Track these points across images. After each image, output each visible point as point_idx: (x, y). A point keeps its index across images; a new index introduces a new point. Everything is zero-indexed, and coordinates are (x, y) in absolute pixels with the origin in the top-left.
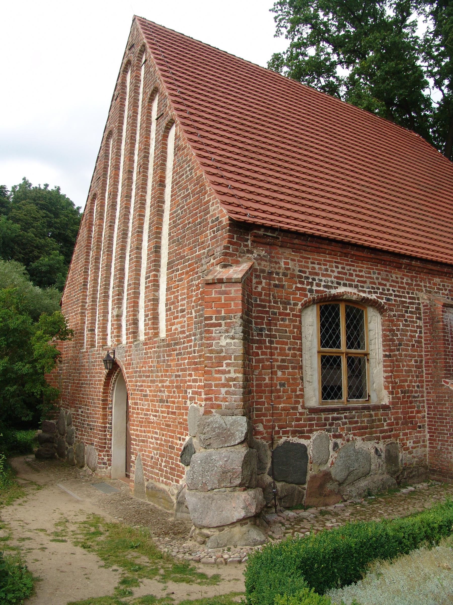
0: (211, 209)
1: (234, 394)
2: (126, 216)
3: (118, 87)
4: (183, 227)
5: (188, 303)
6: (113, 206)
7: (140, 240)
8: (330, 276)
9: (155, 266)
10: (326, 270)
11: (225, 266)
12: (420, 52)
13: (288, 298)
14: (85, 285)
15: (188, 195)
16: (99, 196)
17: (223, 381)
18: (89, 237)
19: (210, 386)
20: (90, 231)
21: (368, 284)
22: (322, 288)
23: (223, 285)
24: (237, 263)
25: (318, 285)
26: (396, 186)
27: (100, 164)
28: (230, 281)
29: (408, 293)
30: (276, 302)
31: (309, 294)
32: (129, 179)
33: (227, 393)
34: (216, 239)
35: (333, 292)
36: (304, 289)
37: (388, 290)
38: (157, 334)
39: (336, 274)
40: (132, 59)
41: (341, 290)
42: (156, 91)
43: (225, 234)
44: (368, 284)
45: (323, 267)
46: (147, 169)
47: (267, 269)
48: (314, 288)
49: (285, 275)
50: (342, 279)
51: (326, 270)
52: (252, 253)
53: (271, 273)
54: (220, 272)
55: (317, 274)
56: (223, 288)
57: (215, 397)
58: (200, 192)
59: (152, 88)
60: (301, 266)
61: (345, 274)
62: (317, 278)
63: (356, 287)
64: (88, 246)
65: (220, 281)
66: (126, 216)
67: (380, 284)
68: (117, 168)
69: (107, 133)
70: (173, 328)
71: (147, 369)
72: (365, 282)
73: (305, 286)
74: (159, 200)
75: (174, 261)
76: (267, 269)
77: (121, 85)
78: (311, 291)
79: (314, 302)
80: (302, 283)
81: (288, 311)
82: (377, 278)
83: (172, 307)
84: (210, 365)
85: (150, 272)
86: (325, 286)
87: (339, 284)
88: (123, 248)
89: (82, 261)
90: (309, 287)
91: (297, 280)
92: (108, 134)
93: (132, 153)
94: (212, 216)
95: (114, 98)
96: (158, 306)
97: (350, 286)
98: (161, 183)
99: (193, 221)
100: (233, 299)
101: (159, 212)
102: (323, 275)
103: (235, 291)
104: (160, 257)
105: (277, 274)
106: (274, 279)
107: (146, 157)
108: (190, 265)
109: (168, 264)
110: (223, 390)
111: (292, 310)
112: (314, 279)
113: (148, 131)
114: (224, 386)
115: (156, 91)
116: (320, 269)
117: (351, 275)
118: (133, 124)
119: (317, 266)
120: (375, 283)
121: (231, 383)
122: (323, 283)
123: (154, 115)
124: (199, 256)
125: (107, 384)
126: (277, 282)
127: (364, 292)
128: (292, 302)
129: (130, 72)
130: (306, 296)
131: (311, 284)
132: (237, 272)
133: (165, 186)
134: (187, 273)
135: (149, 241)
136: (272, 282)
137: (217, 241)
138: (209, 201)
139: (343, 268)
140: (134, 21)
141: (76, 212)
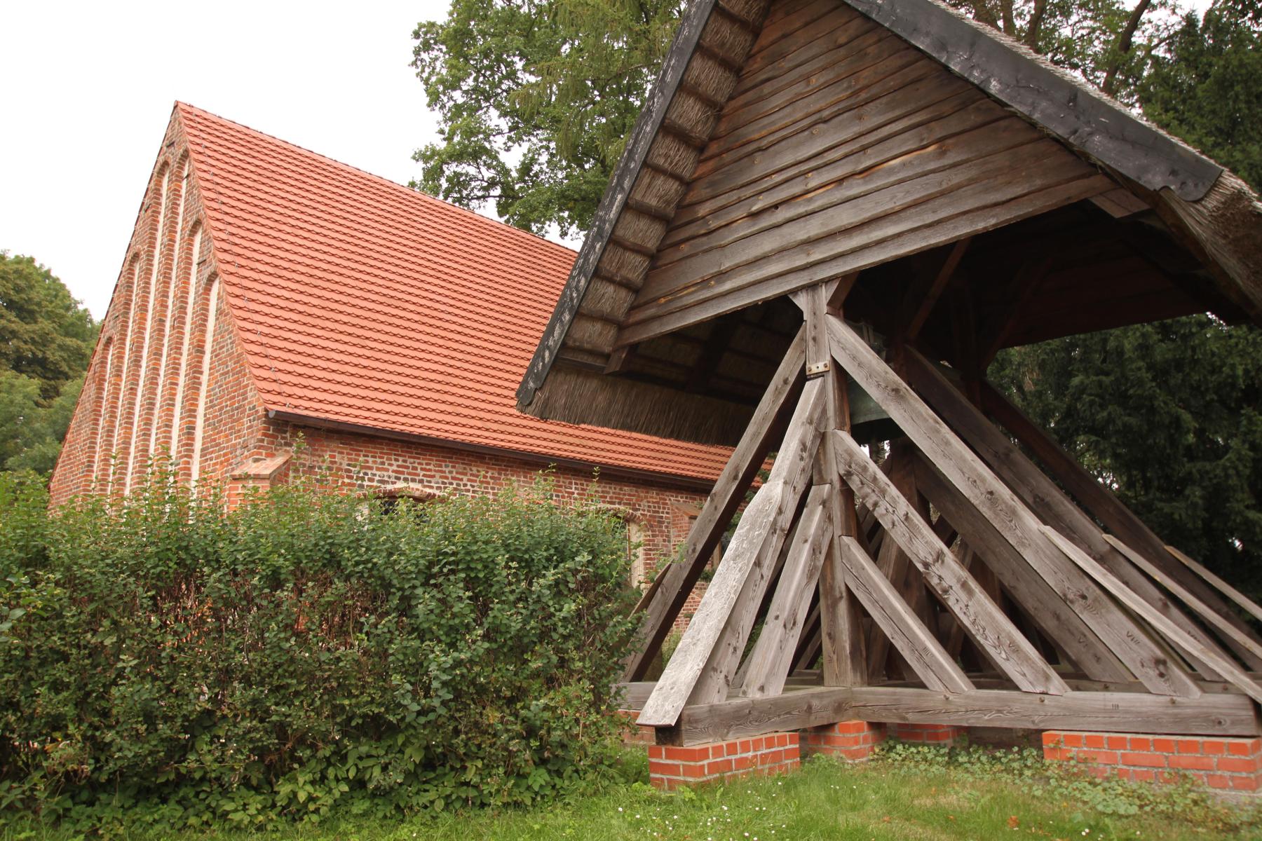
0: (249, 394)
2: (153, 381)
3: (150, 194)
4: (221, 409)
6: (137, 362)
7: (170, 416)
8: (387, 470)
9: (187, 450)
10: (383, 463)
11: (256, 460)
14: (91, 462)
15: (227, 373)
16: (143, 256)
18: (99, 399)
20: (100, 389)
21: (437, 479)
22: (375, 484)
24: (271, 455)
25: (371, 480)
27: (119, 297)
28: (257, 477)
29: (493, 488)
32: (160, 331)
34: (251, 428)
35: (389, 487)
36: (353, 485)
37: (465, 485)
39: (395, 468)
40: (171, 162)
41: (400, 485)
42: (198, 223)
43: (259, 424)
44: (437, 479)
45: (379, 460)
46: (184, 323)
47: (308, 463)
48: (366, 483)
49: (330, 469)
50: (403, 473)
51: (383, 463)
52: (290, 445)
53: (313, 467)
54: (252, 468)
55: (371, 468)
58: (239, 372)
59: (194, 218)
60: (350, 459)
61: (407, 467)
62: (369, 472)
63: (421, 481)
64: (97, 412)
65: (247, 477)
66: (153, 381)
67: (453, 478)
68: (143, 308)
69: (131, 254)
72: (433, 476)
74: (196, 369)
75: (207, 448)
76: (308, 463)
77: (153, 192)
78: (361, 486)
80: (351, 478)
82: (451, 472)
85: (182, 457)
86: (379, 481)
87: (398, 478)
88: (148, 422)
89: (86, 431)
91: (345, 474)
92: (133, 258)
93: (165, 295)
94: (249, 403)
95: (144, 208)
97: (413, 480)
98: (199, 349)
99: (232, 405)
101: (194, 385)
102: (378, 469)
104: (193, 439)
105: (320, 468)
106: (316, 474)
107: (183, 309)
108: (225, 455)
109: (202, 450)
112: (366, 474)
113: (186, 280)
115: (198, 223)
116: (375, 462)
117: (415, 468)
118: (168, 256)
119: (370, 460)
120: (447, 478)
122: (377, 478)
123: (196, 258)
124: (234, 445)
127: (432, 487)
129: (167, 175)
131: (363, 479)
132: (268, 467)
133: (204, 353)
134: (222, 463)
135: (181, 419)
138: (247, 386)
139: (405, 461)
140: (175, 107)
141: (84, 317)
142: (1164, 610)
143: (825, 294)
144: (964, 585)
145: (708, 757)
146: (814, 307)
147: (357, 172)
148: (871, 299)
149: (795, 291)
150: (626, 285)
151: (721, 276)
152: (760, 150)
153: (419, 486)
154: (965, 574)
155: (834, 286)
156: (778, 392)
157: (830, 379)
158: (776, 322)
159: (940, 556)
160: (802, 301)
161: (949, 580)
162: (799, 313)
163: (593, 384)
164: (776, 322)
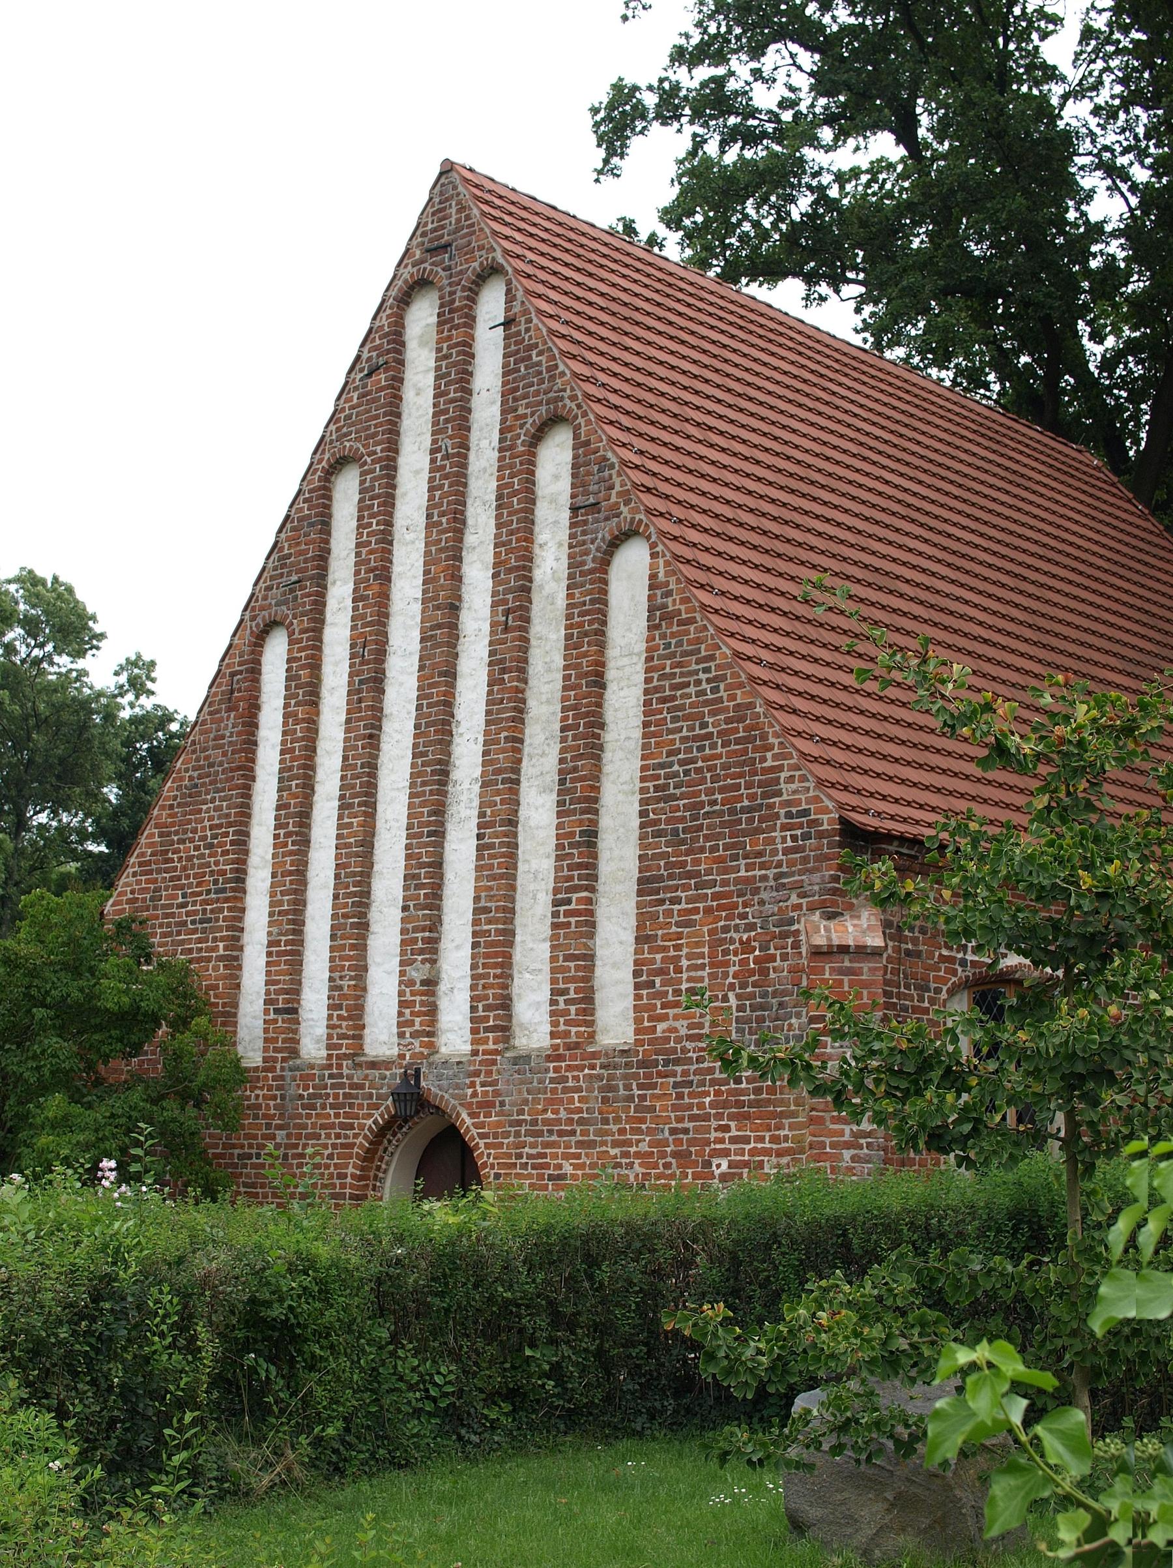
1: (868, 1162)
5: (712, 976)
12: (1111, 276)
13: (926, 979)
17: (847, 1138)
19: (823, 1145)
23: (847, 958)
26: (852, 402)
30: (907, 987)
31: (960, 970)
33: (853, 1159)
38: (505, 1030)
48: (970, 957)
56: (847, 964)
57: (832, 1167)
70: (661, 1027)
71: (563, 1114)
73: (953, 954)
78: (963, 963)
79: (966, 985)
81: (926, 1004)
83: (658, 980)
84: (822, 1107)
90: (960, 955)
96: (593, 972)
100: (865, 985)
103: (870, 969)
105: (911, 929)
110: (847, 1154)
111: (932, 1001)
114: (848, 1145)
121: (862, 1141)
125: (370, 1155)
126: (910, 946)
128: (933, 985)
130: (954, 973)
136: (904, 946)
137: (805, 860)
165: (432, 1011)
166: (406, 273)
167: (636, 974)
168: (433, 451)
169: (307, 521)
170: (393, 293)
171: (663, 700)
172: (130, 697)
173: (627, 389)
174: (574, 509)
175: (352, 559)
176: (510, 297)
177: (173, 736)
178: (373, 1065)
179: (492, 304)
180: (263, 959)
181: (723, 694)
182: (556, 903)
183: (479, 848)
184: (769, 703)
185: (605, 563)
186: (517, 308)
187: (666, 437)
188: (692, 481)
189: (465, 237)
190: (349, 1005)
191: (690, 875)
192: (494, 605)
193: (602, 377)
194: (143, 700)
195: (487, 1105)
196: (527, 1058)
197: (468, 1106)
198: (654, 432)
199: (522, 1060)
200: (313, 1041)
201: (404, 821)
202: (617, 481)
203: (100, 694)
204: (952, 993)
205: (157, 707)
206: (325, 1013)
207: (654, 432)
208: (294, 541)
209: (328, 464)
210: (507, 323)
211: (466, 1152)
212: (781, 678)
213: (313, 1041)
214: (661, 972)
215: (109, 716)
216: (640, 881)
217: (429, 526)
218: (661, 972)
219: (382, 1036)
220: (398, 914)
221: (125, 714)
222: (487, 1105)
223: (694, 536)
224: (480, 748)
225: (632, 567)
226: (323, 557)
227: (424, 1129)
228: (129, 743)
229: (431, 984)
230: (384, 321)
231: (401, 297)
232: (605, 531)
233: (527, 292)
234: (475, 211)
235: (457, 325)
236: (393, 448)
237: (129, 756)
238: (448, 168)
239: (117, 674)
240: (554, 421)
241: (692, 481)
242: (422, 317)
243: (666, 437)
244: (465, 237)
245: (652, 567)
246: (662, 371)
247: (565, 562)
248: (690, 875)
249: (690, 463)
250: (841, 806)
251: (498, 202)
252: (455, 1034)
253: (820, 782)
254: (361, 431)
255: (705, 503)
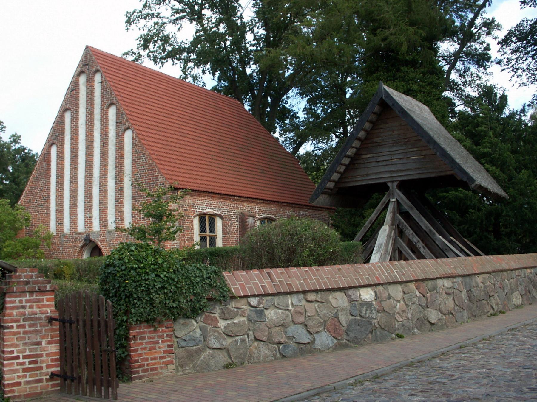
35: (205, 211)
38: (106, 226)
41: (207, 210)
48: (198, 210)
78: (197, 211)
79: (197, 215)
125: (80, 251)
142: (461, 252)
143: (395, 184)
144: (424, 247)
145: (25, 340)
146: (393, 186)
147: (111, 56)
148: (404, 186)
149: (388, 182)
150: (340, 173)
151: (367, 175)
152: (379, 145)
153: (212, 211)
154: (423, 245)
155: (397, 182)
156: (382, 204)
157: (396, 203)
158: (382, 188)
159: (418, 241)
160: (389, 184)
161: (420, 246)
162: (389, 187)
163: (326, 196)
164: (382, 188)
165: (91, 223)
166: (79, 69)
167: (132, 215)
168: (87, 109)
169: (59, 123)
170: (76, 73)
171: (136, 162)
172: (14, 144)
173: (128, 97)
174: (117, 123)
175: (70, 131)
176: (102, 77)
177: (26, 153)
178: (80, 234)
179: (98, 78)
180: (55, 213)
181: (147, 161)
182: (116, 201)
183: (100, 191)
184: (156, 163)
185: (123, 134)
186: (103, 80)
187: (136, 107)
188: (141, 116)
189: (92, 62)
190: (74, 222)
191: (142, 196)
192: (101, 142)
193: (122, 95)
194: (17, 144)
195: (103, 241)
196: (111, 232)
197: (100, 241)
198: (133, 106)
199: (110, 232)
200: (67, 228)
201: (84, 185)
202: (125, 117)
203: (6, 143)
204: (194, 217)
205: (21, 146)
206: (69, 224)
207: (133, 106)
208: (57, 126)
209: (64, 110)
210: (101, 83)
211: (100, 250)
212: (159, 158)
213: (67, 228)
214: (137, 214)
215: (9, 148)
216: (132, 197)
217: (86, 124)
218: (137, 214)
219: (81, 227)
220: (83, 204)
221: (13, 148)
222: (103, 241)
223: (141, 128)
224: (99, 171)
225: (128, 136)
226: (63, 131)
227: (91, 246)
228: (14, 155)
229: (91, 218)
230: (74, 79)
231: (79, 73)
232: (123, 127)
233: (105, 76)
234: (94, 58)
235: (90, 81)
236: (78, 107)
237: (14, 159)
238: (87, 47)
239: (10, 138)
240: (112, 104)
241: (141, 116)
242: (82, 79)
243: (136, 107)
244: (92, 62)
245: (133, 135)
246: (136, 92)
247: (115, 133)
248: (142, 196)
249: (141, 112)
250: (170, 183)
251: (99, 55)
252: (96, 227)
253: (166, 179)
254: (70, 103)
255: (144, 121)
